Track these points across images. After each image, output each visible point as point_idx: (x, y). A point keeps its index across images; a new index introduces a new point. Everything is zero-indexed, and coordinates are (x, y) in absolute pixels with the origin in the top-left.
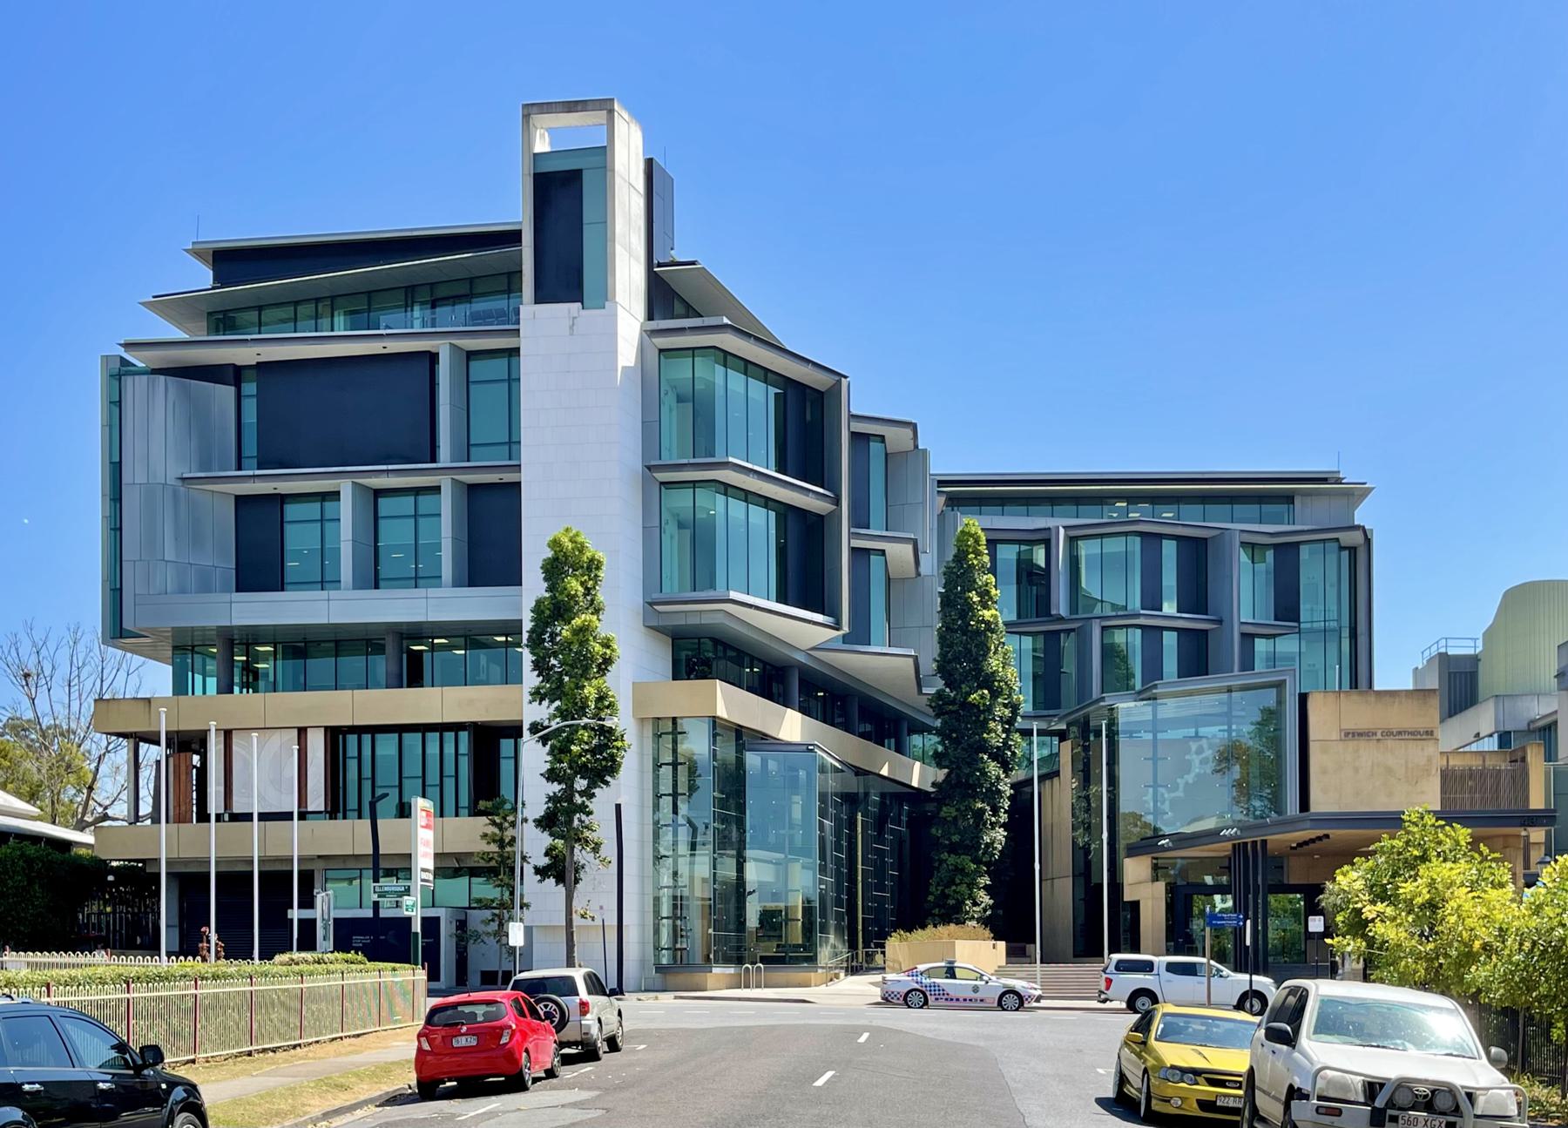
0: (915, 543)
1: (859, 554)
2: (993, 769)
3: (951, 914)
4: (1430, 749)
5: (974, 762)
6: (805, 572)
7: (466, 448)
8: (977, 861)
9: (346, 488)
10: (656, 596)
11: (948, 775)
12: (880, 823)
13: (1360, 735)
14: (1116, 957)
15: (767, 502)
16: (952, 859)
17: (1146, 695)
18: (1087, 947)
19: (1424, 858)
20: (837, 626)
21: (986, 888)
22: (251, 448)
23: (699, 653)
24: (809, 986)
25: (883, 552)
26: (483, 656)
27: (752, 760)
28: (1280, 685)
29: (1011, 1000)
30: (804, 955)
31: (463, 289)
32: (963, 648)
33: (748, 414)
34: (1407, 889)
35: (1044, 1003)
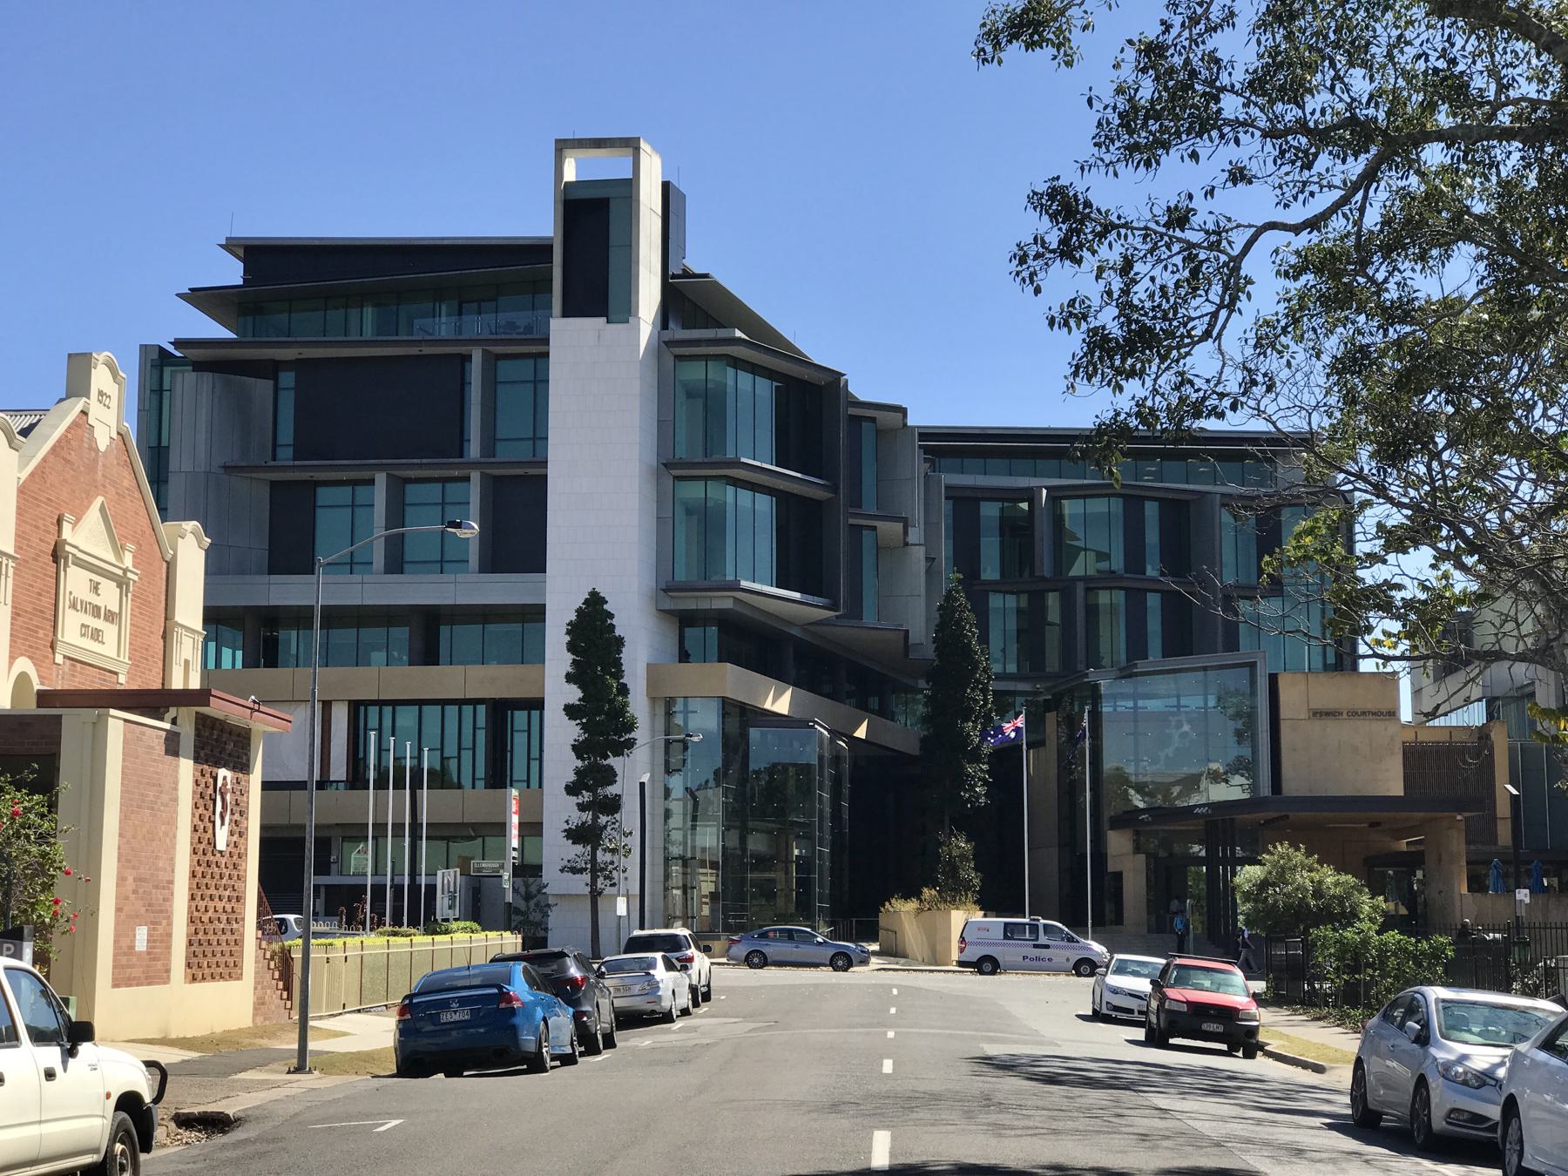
9: (381, 479)
13: (1327, 714)
17: (1127, 674)
25: (875, 528)
27: (754, 733)
28: (1252, 666)
33: (752, 400)
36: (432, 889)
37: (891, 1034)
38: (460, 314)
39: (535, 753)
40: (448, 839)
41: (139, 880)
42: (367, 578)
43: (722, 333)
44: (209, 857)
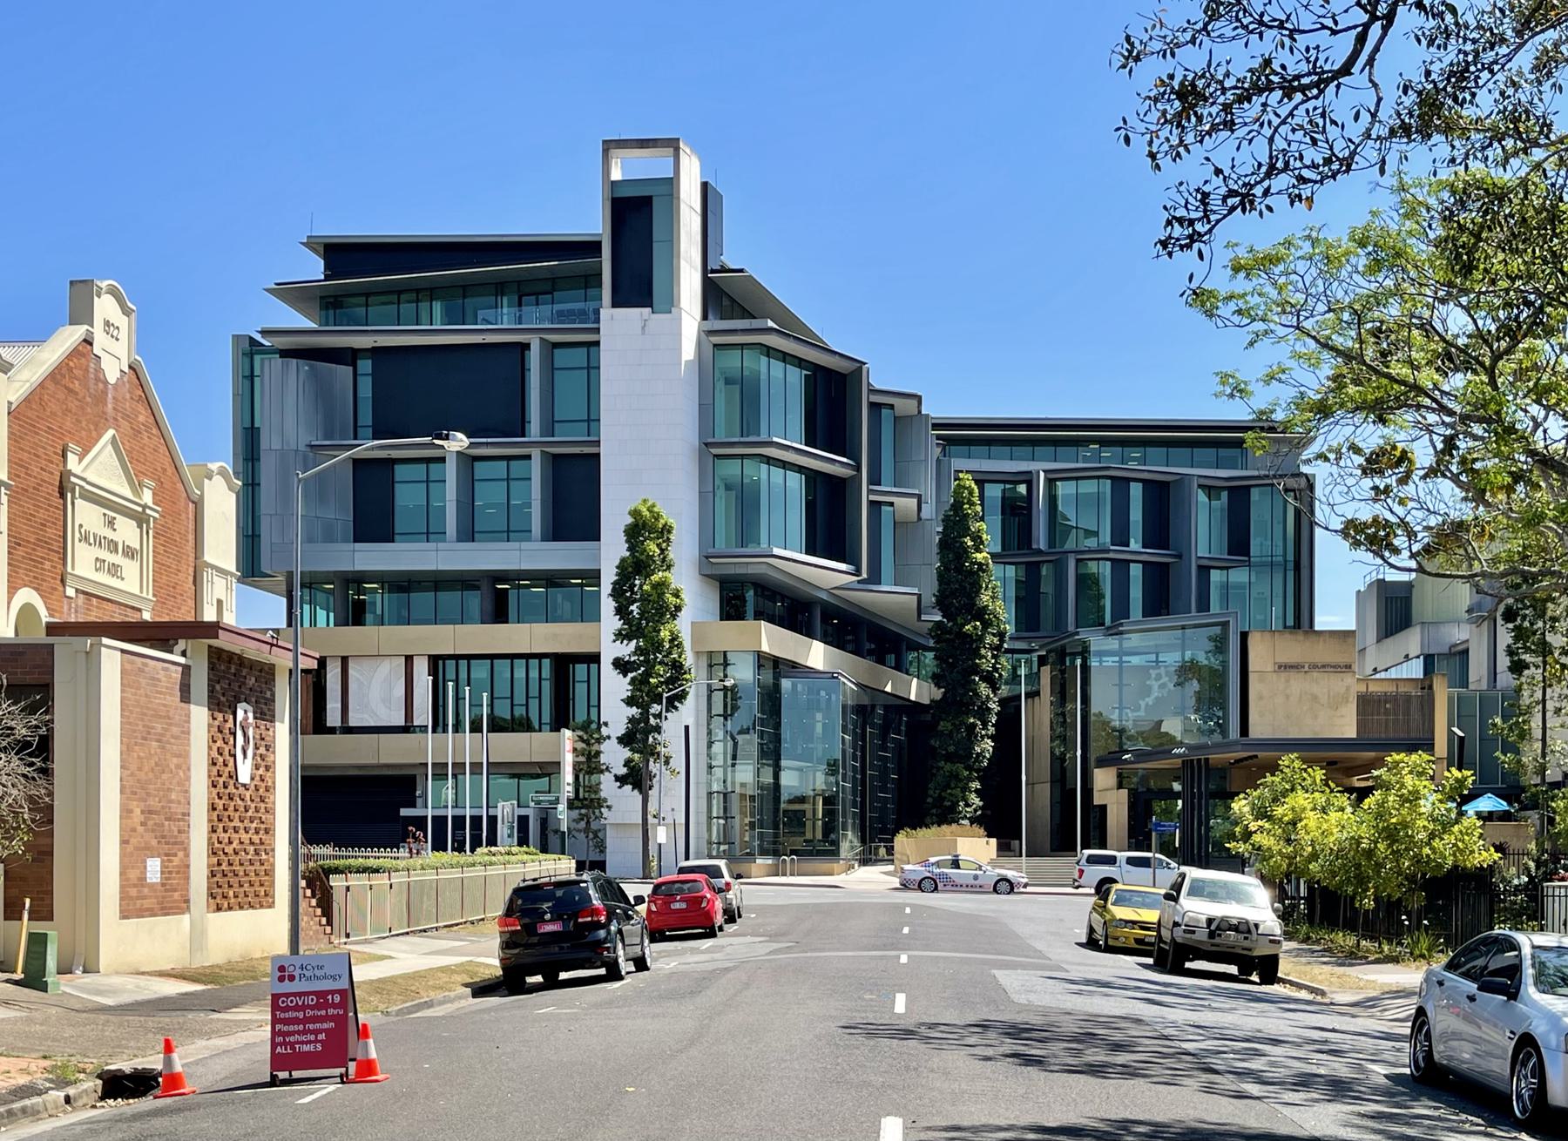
0: (919, 497)
1: (875, 506)
2: (984, 689)
3: (947, 816)
4: (1349, 680)
5: (970, 686)
6: (830, 526)
7: (549, 426)
8: (969, 768)
10: (711, 550)
11: (945, 694)
12: (885, 730)
14: (1087, 852)
15: (800, 469)
16: (948, 767)
17: (1114, 631)
18: (1062, 843)
19: (1293, 790)
20: (858, 573)
21: (977, 791)
22: (366, 417)
23: (740, 596)
24: (831, 874)
26: (558, 594)
27: (786, 684)
28: (1225, 625)
29: (1004, 886)
30: (824, 849)
31: (548, 287)
32: (958, 586)
33: (785, 393)
34: (1279, 811)
35: (1029, 889)
36: (493, 820)
37: (904, 959)
38: (520, 305)
39: (594, 702)
40: (519, 776)
41: (148, 812)
42: (441, 545)
43: (756, 324)
44: (231, 789)
